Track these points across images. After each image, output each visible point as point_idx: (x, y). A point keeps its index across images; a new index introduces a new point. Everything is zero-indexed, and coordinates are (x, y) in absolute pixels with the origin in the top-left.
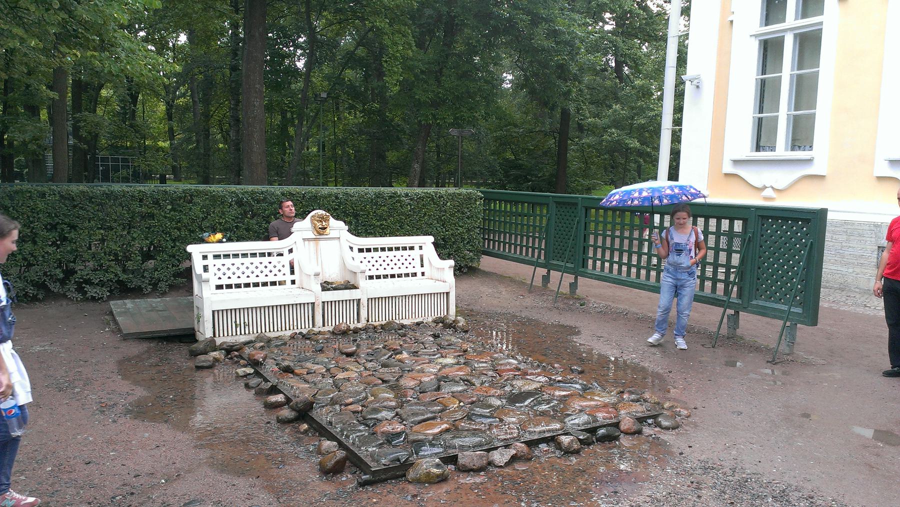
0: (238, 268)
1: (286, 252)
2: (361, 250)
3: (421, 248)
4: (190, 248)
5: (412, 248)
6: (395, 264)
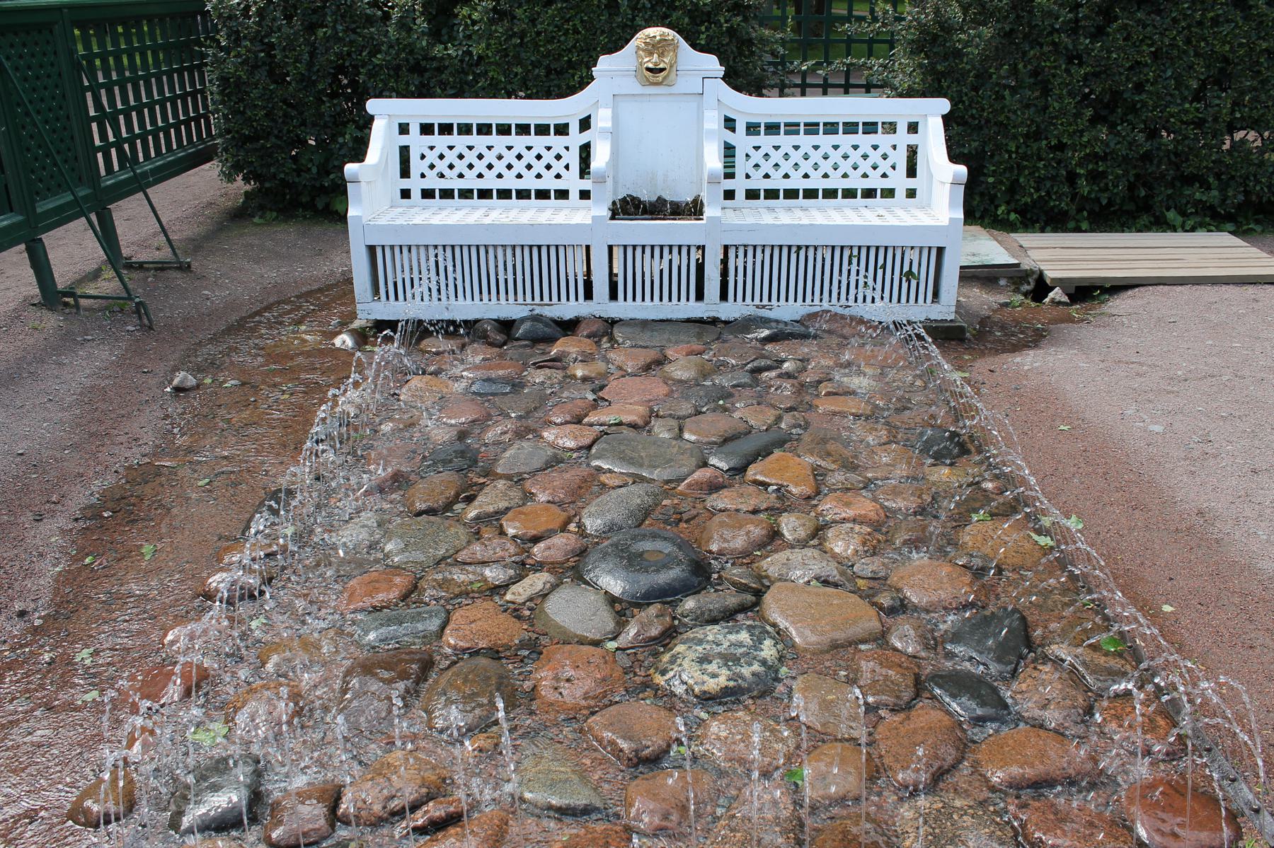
1: (574, 127)
4: (373, 106)
5: (891, 128)
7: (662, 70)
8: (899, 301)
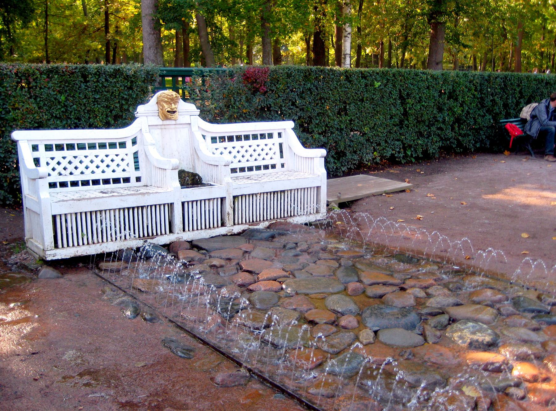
0: (92, 162)
3: (280, 135)
4: (17, 135)
5: (270, 136)
8: (68, 246)
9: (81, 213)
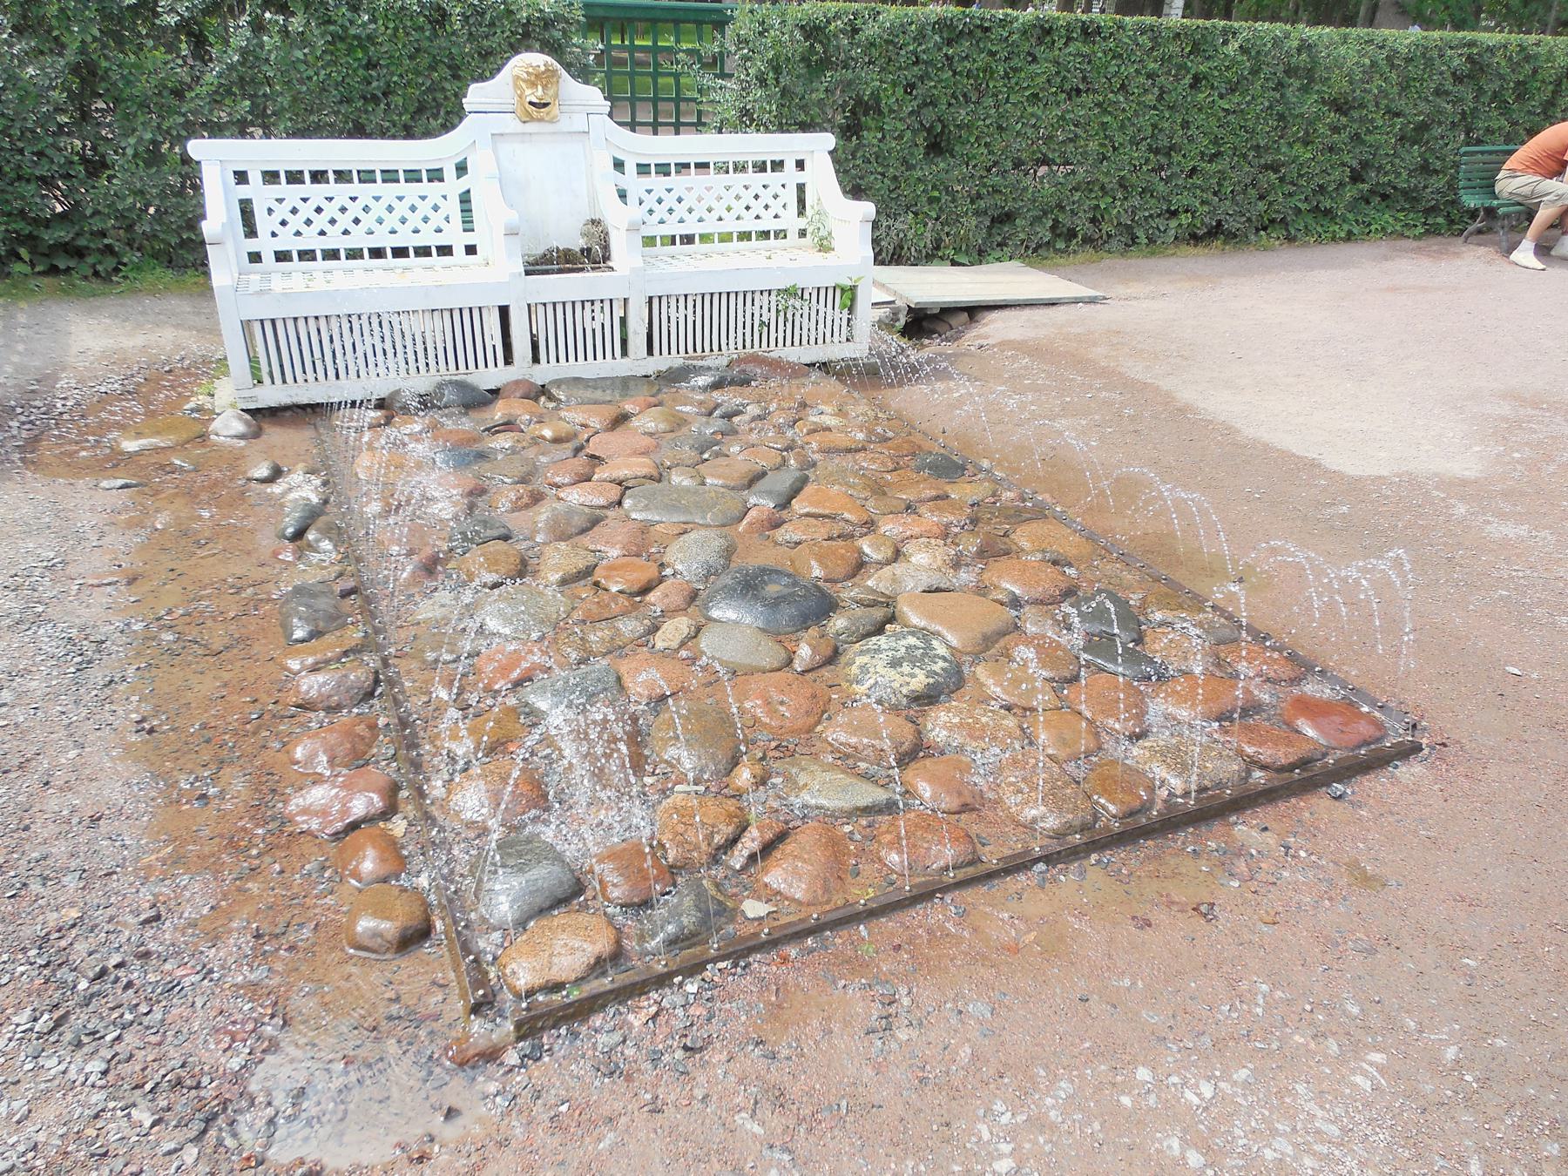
1: (450, 172)
2: (643, 169)
3: (800, 165)
4: (197, 148)
5: (778, 165)
6: (748, 208)
7: (546, 105)
9: (712, 294)
